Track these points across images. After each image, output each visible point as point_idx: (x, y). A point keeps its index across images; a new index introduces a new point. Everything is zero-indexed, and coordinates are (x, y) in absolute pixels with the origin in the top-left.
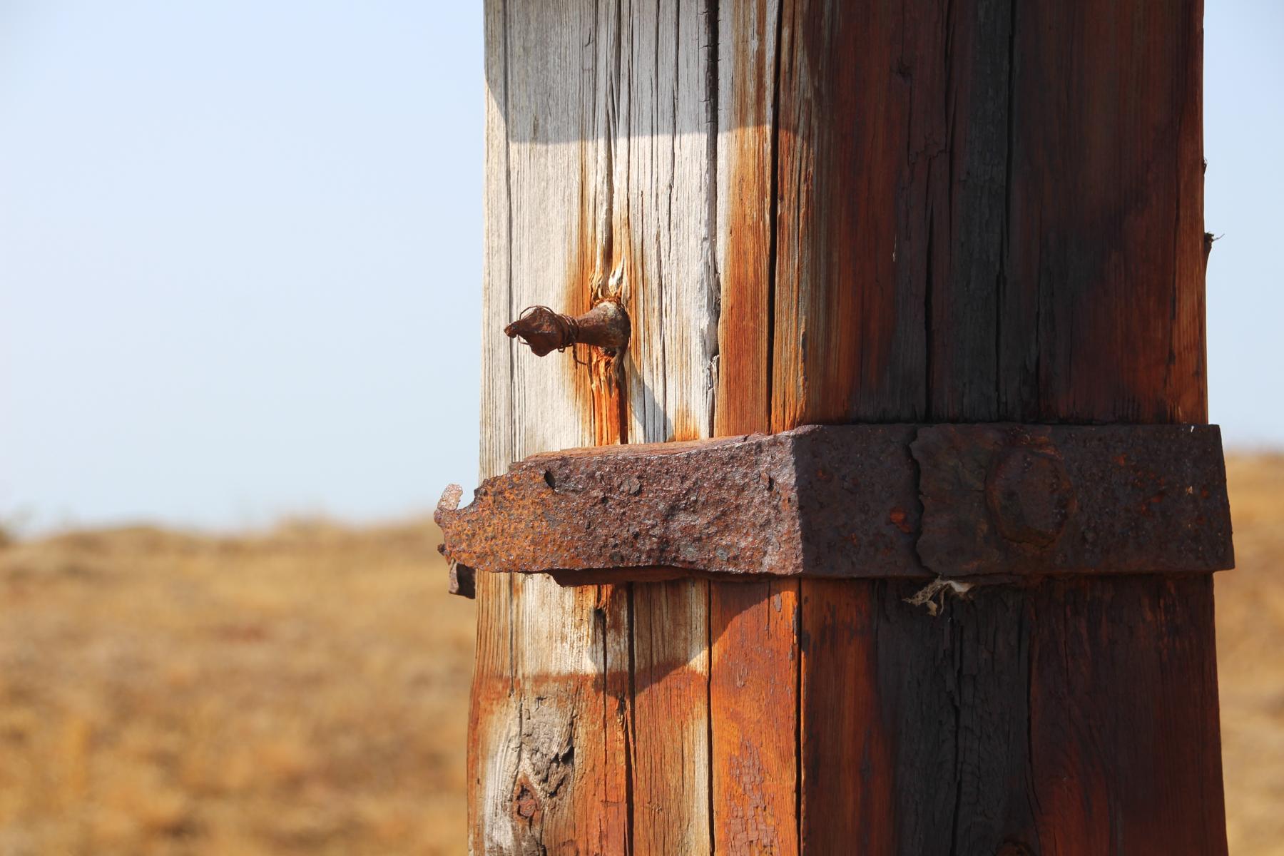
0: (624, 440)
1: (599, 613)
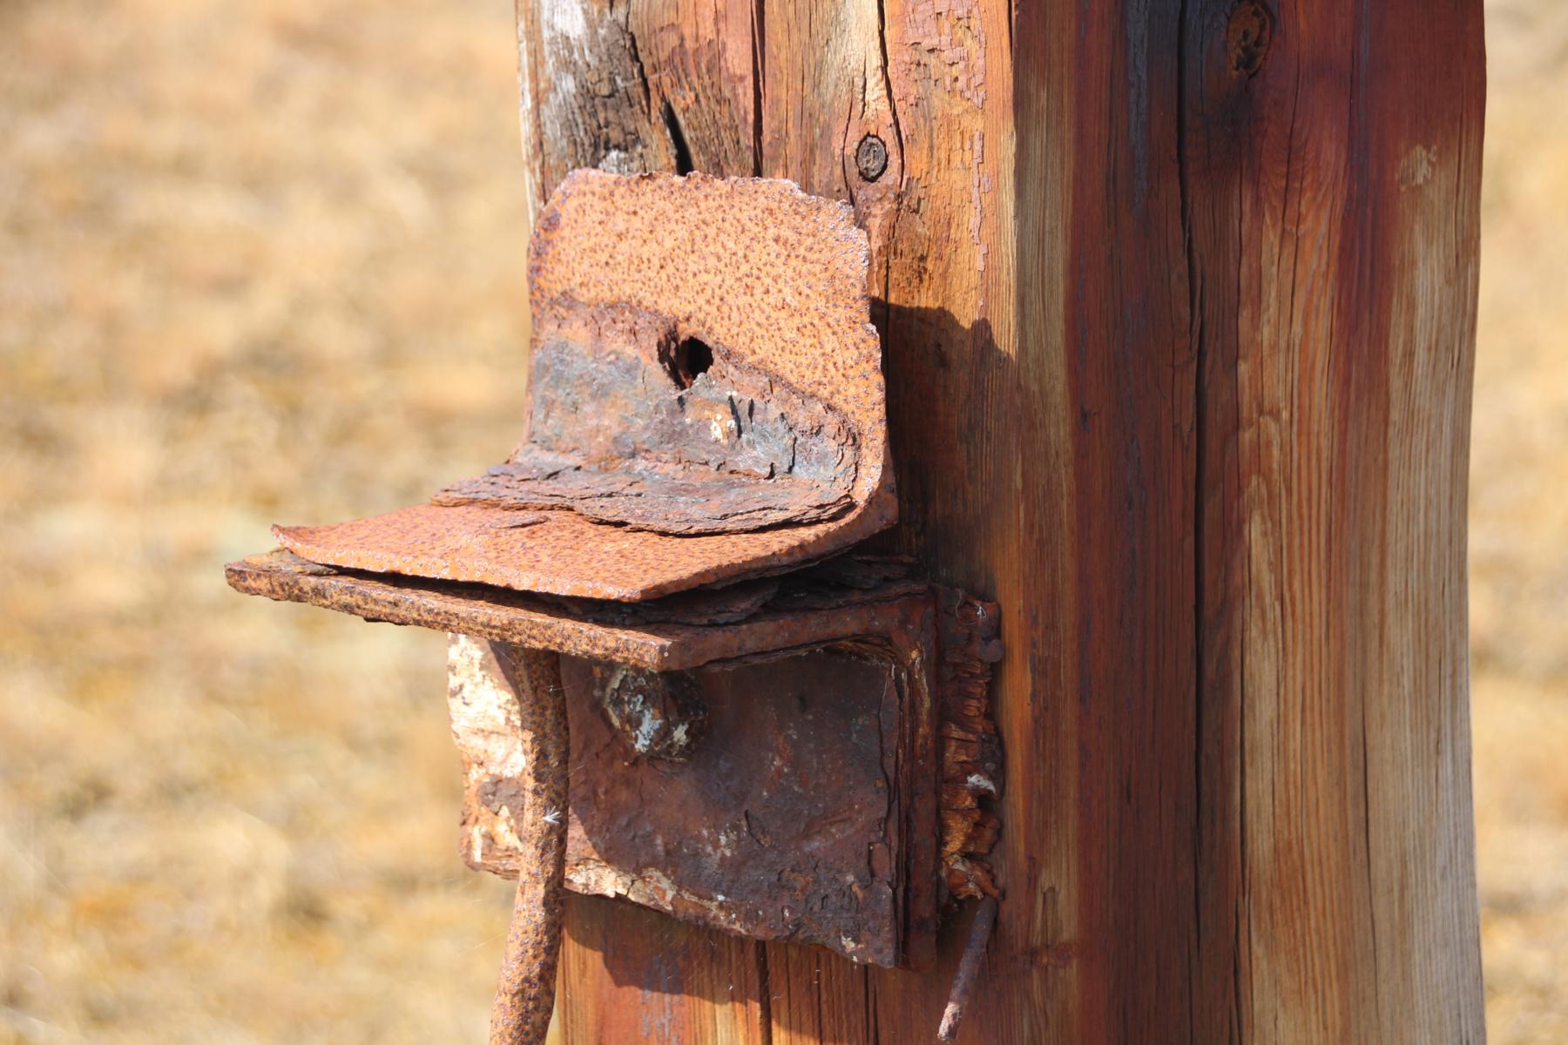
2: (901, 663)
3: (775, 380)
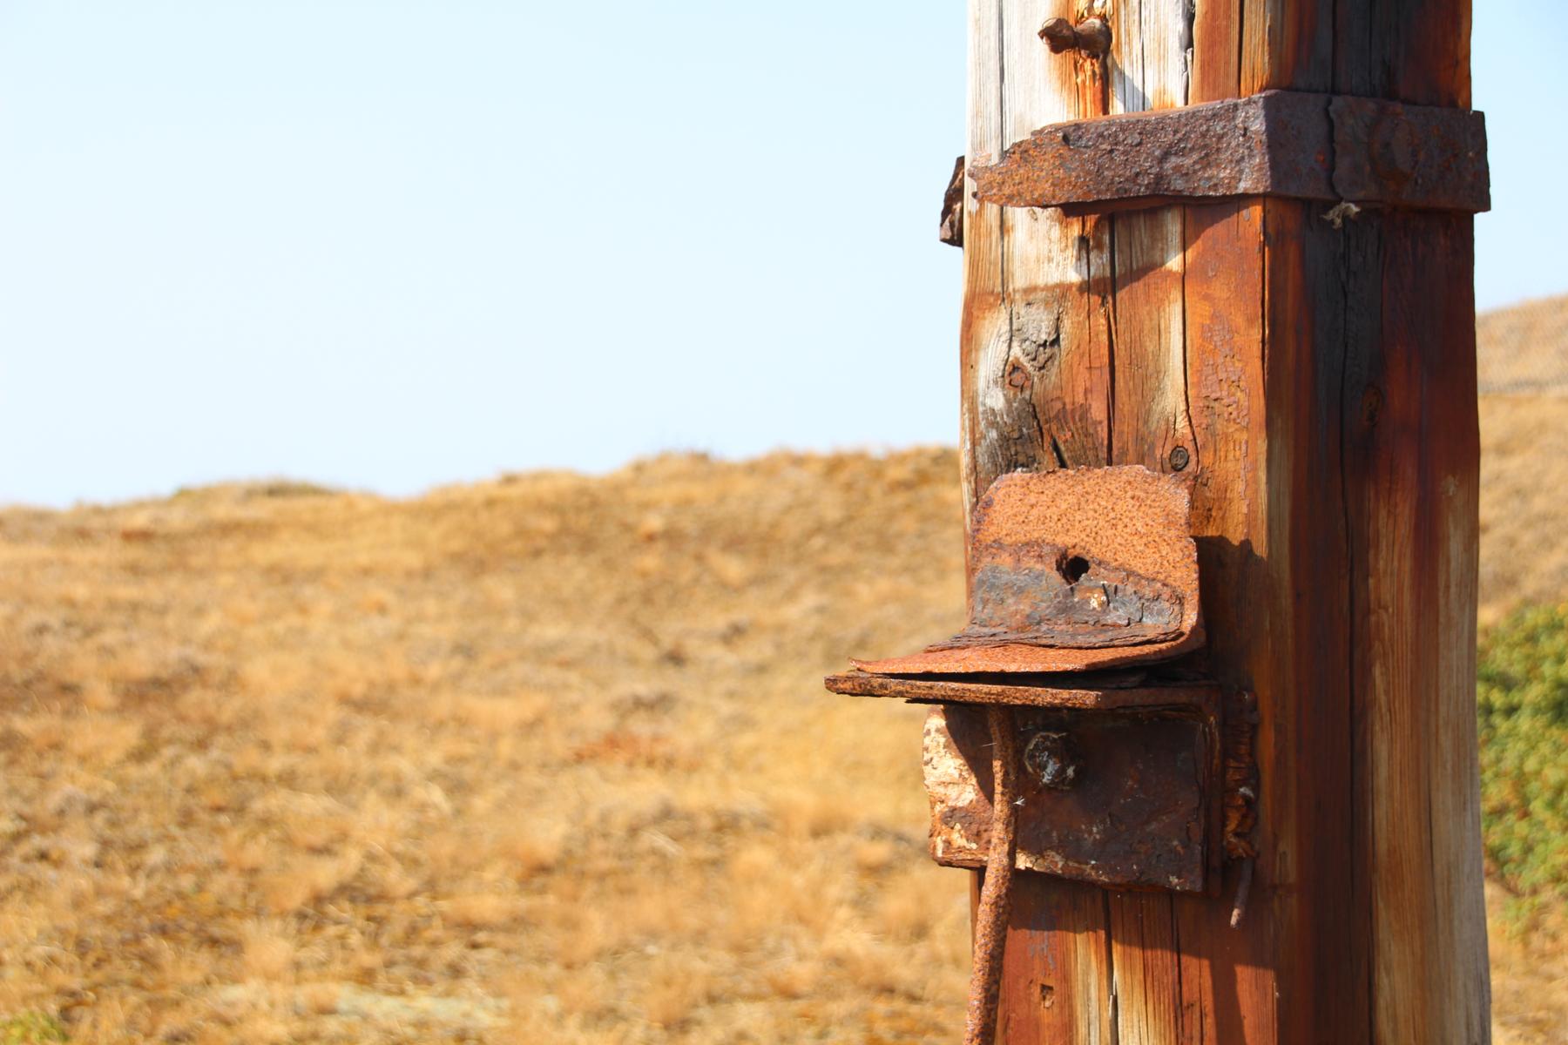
0: (1106, 112)
1: (1083, 240)
2: (1206, 723)
3: (1130, 573)
